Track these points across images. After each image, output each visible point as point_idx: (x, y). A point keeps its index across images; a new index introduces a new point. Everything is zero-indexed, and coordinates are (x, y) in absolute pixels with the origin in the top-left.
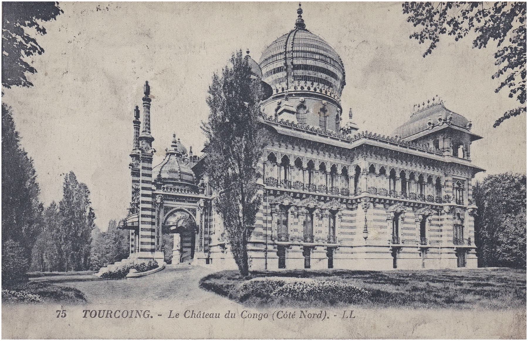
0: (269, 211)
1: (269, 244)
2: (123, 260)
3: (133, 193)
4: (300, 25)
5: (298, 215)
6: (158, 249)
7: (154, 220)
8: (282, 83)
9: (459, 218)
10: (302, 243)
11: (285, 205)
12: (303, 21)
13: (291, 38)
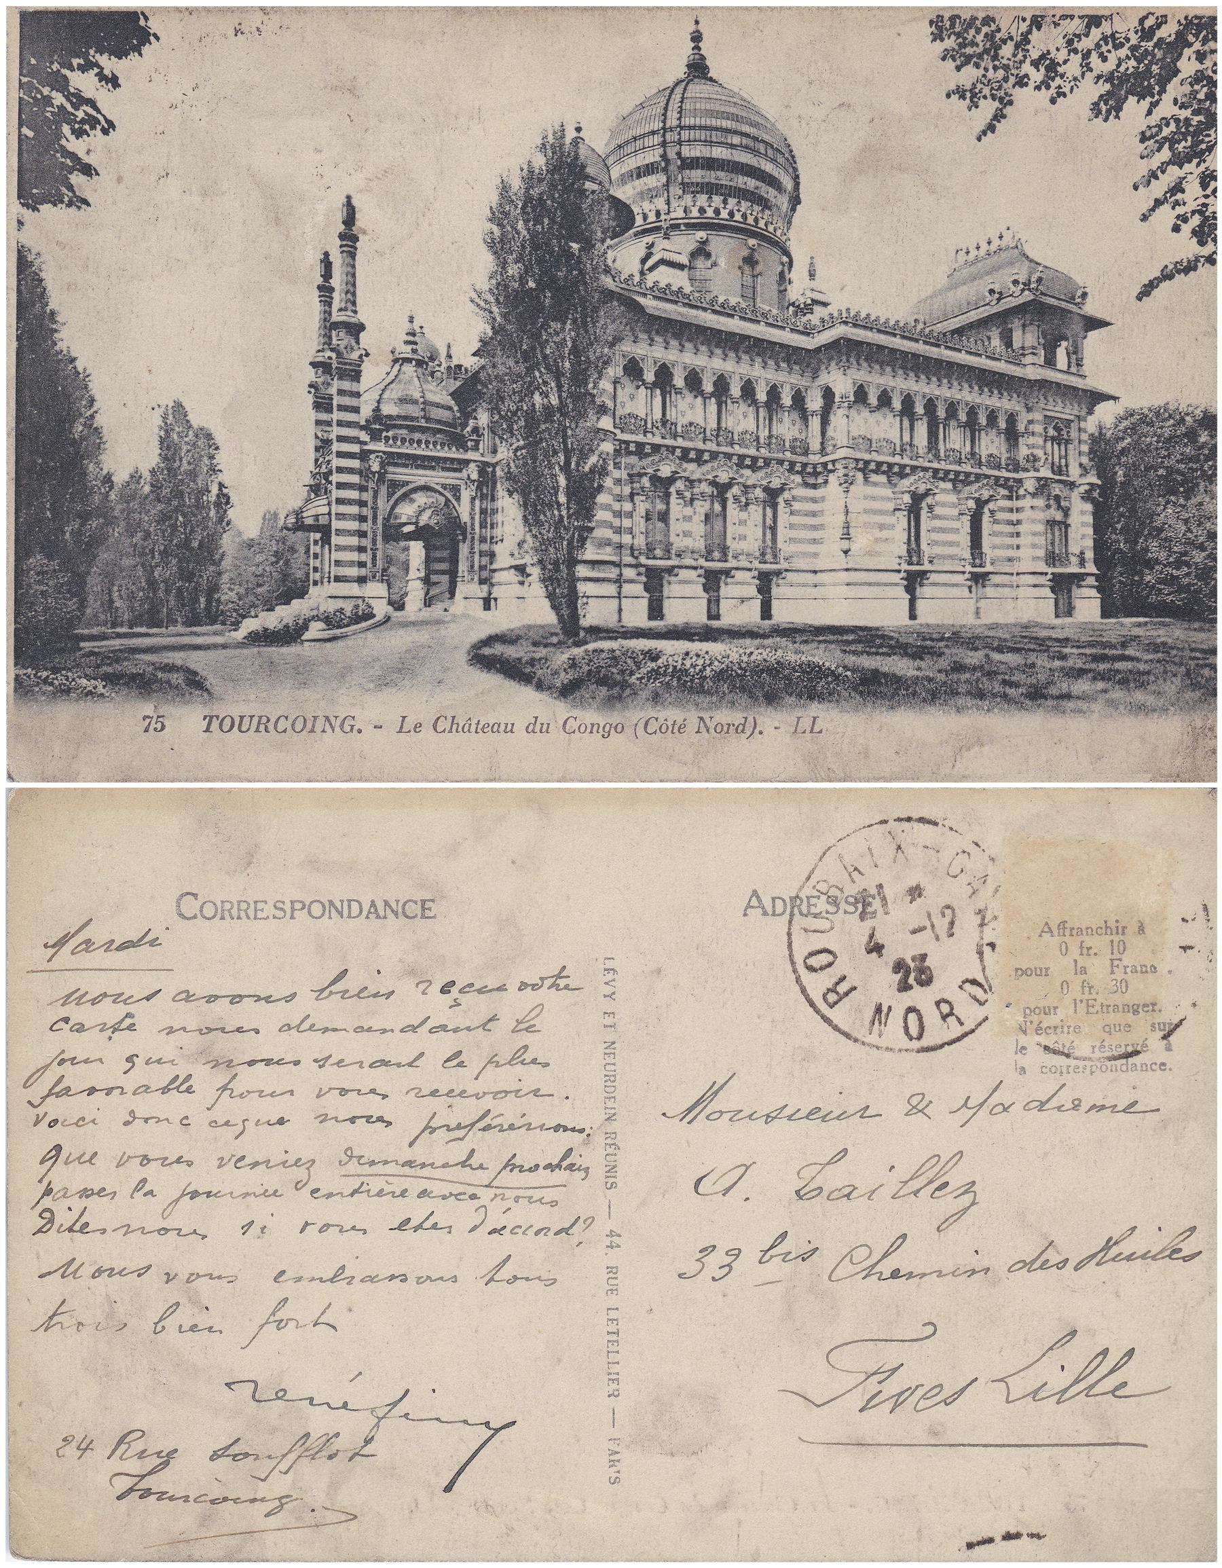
0: (627, 490)
1: (626, 565)
2: (294, 601)
3: (317, 449)
7: (365, 511)
8: (655, 200)
9: (1059, 507)
10: (702, 562)
11: (664, 476)
12: (703, 58)
13: (677, 96)
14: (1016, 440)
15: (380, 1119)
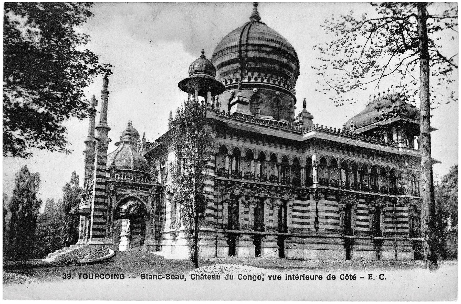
0: (220, 200)
1: (219, 233)
3: (86, 179)
4: (256, 18)
5: (273, 206)
6: (109, 235)
7: (106, 207)
8: (236, 74)
9: (416, 211)
10: (253, 231)
11: (236, 194)
12: (257, 13)
14: (395, 181)
15: (373, 5)
